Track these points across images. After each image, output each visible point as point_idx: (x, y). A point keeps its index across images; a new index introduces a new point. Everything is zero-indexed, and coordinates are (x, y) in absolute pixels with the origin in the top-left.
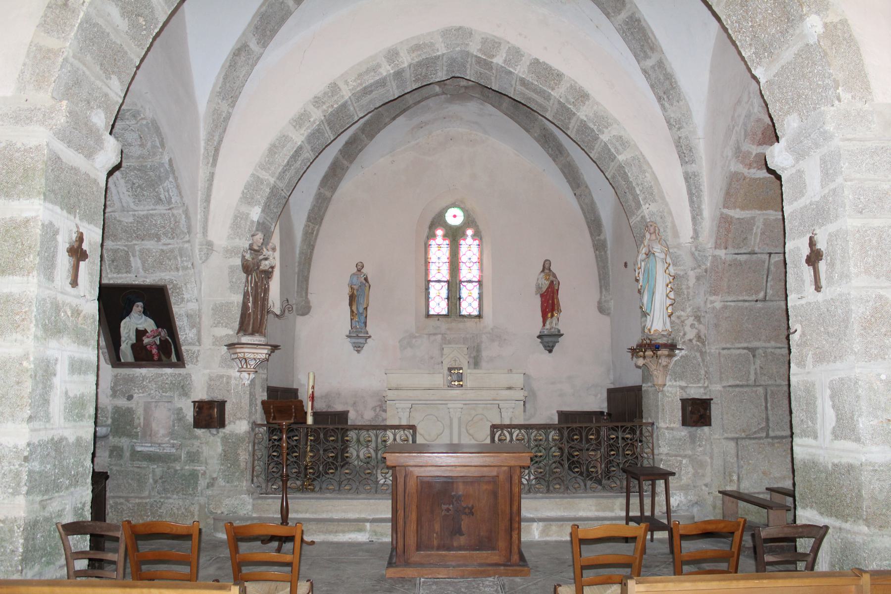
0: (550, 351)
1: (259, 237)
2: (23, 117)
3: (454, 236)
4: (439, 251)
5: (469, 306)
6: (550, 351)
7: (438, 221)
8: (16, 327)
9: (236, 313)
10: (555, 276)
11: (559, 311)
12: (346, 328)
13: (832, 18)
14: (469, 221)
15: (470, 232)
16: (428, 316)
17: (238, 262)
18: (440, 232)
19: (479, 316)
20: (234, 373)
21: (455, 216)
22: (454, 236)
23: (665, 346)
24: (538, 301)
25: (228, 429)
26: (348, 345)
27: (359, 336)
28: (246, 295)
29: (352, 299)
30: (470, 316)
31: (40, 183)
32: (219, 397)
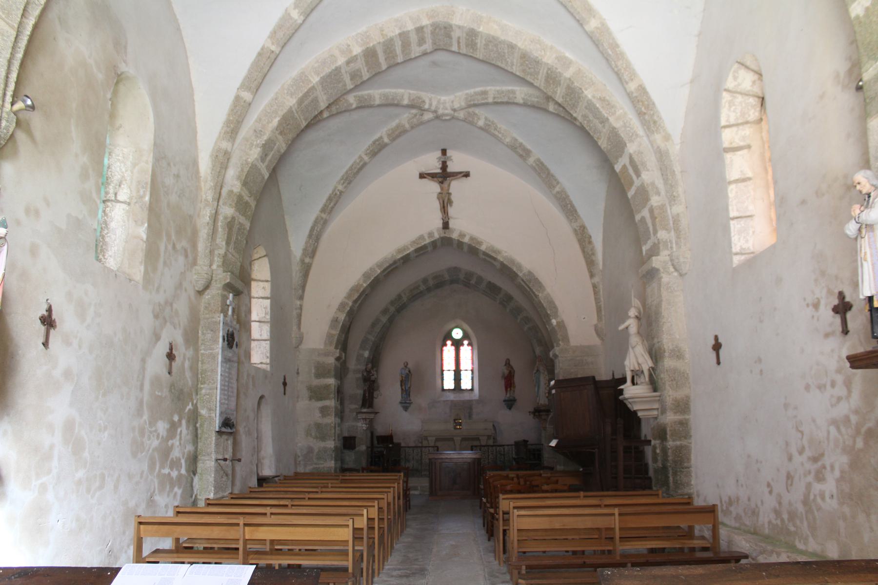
0: (510, 409)
1: (370, 366)
2: (327, 354)
3: (457, 344)
4: (449, 351)
5: (466, 384)
6: (510, 409)
7: (448, 336)
8: (329, 415)
9: (360, 398)
10: (512, 368)
11: (514, 387)
12: (399, 398)
13: (559, 320)
14: (466, 336)
15: (466, 342)
16: (443, 390)
17: (360, 375)
18: (449, 343)
19: (472, 390)
20: (359, 424)
21: (457, 334)
22: (457, 344)
23: (544, 411)
24: (503, 382)
25: (357, 449)
26: (400, 408)
27: (406, 404)
28: (365, 391)
29: (402, 383)
30: (466, 390)
31: (333, 373)
32: (354, 435)
